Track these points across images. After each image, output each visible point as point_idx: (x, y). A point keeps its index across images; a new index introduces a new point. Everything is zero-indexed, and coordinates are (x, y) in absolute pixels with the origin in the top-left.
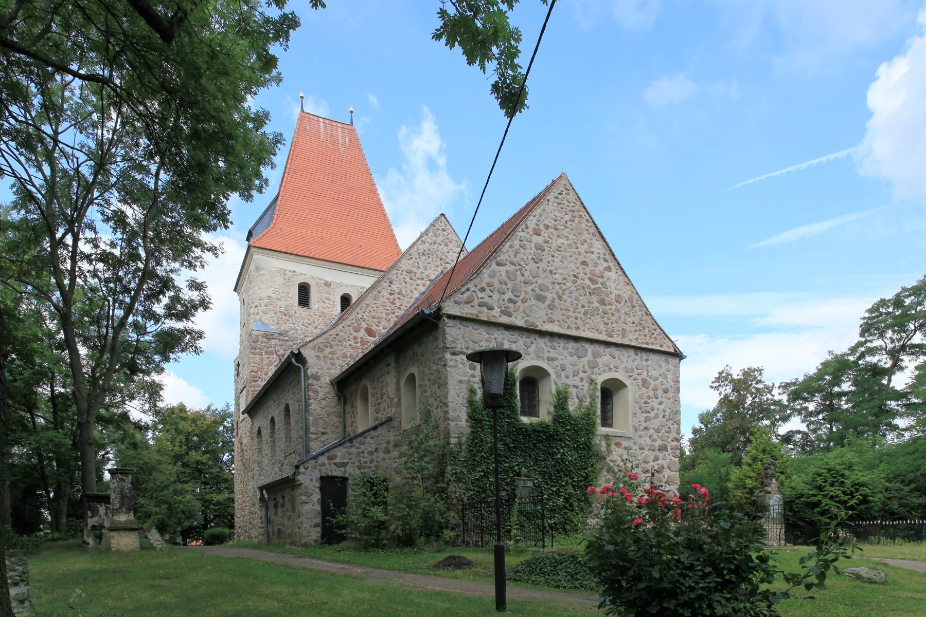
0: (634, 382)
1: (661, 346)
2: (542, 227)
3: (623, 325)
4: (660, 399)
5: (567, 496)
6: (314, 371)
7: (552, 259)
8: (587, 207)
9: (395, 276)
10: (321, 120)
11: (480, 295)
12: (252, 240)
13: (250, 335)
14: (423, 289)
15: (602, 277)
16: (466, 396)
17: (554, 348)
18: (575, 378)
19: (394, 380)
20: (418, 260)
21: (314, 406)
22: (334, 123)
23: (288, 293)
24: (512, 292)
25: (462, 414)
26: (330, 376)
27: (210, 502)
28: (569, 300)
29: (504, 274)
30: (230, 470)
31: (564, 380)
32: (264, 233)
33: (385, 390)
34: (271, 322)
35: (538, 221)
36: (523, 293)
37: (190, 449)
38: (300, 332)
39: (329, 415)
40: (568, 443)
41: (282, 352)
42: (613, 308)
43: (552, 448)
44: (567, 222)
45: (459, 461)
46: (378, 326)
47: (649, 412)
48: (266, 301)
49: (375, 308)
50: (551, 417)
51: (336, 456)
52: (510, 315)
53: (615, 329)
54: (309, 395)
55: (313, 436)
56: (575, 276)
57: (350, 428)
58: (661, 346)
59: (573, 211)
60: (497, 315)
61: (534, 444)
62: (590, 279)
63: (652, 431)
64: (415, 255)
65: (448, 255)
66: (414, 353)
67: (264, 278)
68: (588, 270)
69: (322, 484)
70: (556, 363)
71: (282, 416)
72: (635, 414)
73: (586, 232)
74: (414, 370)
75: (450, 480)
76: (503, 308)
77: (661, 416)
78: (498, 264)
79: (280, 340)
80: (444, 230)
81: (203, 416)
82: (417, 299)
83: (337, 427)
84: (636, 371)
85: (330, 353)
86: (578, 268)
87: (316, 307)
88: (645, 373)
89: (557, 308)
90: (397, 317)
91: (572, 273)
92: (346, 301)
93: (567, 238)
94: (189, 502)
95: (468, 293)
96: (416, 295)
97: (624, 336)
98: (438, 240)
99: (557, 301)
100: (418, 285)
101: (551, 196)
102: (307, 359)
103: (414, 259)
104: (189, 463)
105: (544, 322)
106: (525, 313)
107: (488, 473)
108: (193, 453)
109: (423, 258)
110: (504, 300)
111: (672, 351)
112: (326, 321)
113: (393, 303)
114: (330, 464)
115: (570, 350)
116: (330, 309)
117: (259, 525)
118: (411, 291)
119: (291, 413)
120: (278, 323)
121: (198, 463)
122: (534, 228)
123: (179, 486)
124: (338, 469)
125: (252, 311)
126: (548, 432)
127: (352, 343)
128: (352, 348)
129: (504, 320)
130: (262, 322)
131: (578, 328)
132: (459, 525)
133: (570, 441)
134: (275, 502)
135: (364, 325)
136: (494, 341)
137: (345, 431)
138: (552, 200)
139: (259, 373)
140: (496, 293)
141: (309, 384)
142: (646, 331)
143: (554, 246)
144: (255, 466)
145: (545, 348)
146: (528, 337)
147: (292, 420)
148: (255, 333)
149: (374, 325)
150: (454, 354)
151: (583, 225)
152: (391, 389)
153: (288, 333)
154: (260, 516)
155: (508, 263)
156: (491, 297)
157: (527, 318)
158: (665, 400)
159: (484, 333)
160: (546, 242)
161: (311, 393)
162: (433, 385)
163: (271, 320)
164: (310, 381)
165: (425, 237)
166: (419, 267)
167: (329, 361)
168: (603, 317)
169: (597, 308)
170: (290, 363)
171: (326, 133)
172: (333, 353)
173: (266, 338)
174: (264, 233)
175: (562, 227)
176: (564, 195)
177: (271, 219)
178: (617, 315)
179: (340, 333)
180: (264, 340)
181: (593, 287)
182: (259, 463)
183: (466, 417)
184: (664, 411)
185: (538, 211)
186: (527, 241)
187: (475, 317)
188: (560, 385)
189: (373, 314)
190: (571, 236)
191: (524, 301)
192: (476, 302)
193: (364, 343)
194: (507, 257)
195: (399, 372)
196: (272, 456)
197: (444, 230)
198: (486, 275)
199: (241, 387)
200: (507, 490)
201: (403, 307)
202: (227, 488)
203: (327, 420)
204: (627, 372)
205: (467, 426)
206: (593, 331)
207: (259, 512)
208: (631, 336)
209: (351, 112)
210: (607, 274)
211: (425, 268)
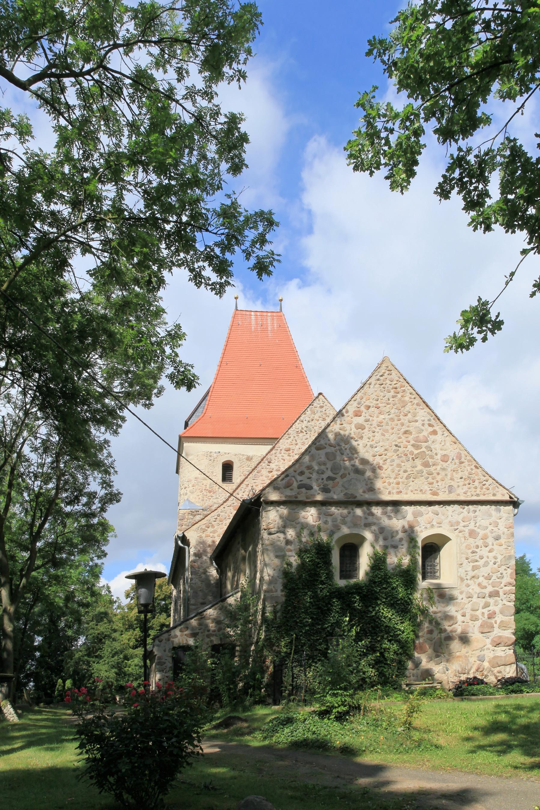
0: (460, 534)
1: (494, 495)
2: (362, 408)
3: (450, 481)
4: (490, 547)
8: (409, 382)
9: (273, 456)
11: (299, 478)
15: (426, 441)
23: (212, 472)
24: (331, 470)
28: (391, 468)
36: (343, 470)
42: (439, 467)
47: (477, 561)
48: (193, 482)
55: (193, 607)
56: (396, 446)
58: (494, 495)
63: (481, 579)
72: (461, 564)
77: (491, 563)
80: (322, 407)
84: (462, 524)
86: (400, 438)
88: (473, 523)
91: (394, 443)
93: (389, 413)
97: (450, 492)
98: (316, 417)
103: (292, 438)
106: (344, 487)
109: (301, 435)
110: (323, 479)
111: (507, 498)
120: (203, 500)
122: (355, 412)
130: (189, 501)
131: (401, 492)
142: (476, 483)
158: (496, 547)
160: (367, 421)
166: (297, 444)
168: (427, 478)
169: (421, 470)
171: (257, 324)
178: (443, 473)
179: (221, 514)
181: (416, 452)
183: (282, 588)
184: (495, 558)
187: (294, 499)
191: (343, 476)
197: (322, 407)
204: (452, 526)
205: (282, 595)
206: (416, 492)
210: (432, 437)
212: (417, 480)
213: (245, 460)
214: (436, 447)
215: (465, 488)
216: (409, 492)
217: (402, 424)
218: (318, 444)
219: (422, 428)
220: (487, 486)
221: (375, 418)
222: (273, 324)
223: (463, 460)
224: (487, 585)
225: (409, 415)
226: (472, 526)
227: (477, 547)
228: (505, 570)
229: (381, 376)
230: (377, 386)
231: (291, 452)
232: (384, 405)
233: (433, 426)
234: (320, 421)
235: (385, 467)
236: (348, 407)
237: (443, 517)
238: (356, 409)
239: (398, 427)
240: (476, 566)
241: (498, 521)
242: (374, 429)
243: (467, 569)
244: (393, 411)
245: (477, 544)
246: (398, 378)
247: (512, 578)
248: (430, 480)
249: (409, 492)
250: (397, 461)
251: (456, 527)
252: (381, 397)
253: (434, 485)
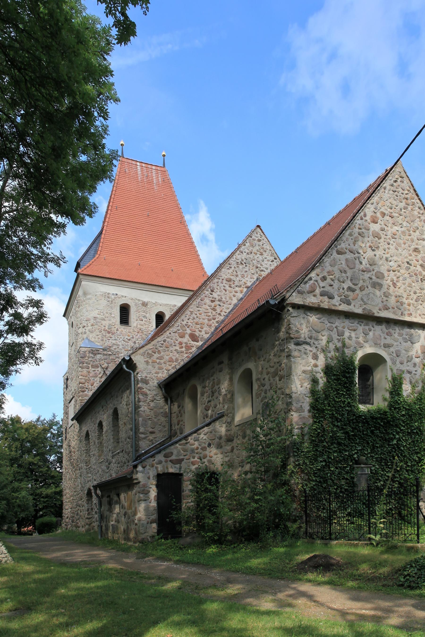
2: (378, 215)
5: (402, 481)
6: (144, 376)
7: (388, 246)
8: (419, 194)
9: (216, 284)
10: (138, 164)
11: (322, 284)
12: (79, 271)
13: (79, 352)
14: (241, 296)
16: (309, 386)
18: (409, 363)
19: (228, 377)
20: (237, 269)
21: (144, 408)
22: (149, 166)
23: (111, 314)
24: (351, 280)
25: (304, 404)
26: (158, 380)
27: (40, 495)
28: (403, 287)
29: (344, 262)
30: (56, 468)
31: (399, 366)
32: (91, 262)
33: (216, 387)
34: (97, 340)
35: (376, 209)
37: (23, 453)
38: (121, 347)
39: (156, 416)
40: (402, 428)
41: (105, 365)
43: (388, 434)
44: (401, 209)
45: (302, 452)
46: (200, 331)
49: (198, 315)
50: (386, 403)
51: (172, 453)
52: (349, 304)
54: (139, 398)
55: (142, 436)
56: (408, 263)
57: (177, 427)
59: (407, 199)
60: (337, 304)
61: (372, 432)
62: (421, 265)
64: (234, 264)
65: (262, 263)
66: (250, 349)
67: (91, 302)
68: (419, 256)
69: (158, 481)
70: (392, 349)
71: (111, 419)
73: (418, 219)
74: (251, 365)
75: (293, 472)
76: (343, 297)
78: (339, 253)
79: (104, 355)
80: (259, 241)
81: (34, 425)
82: (236, 305)
83: (164, 426)
85: (157, 359)
86: (410, 255)
87: (135, 325)
89: (391, 296)
90: (217, 322)
91: (406, 260)
92: (160, 317)
94: (23, 497)
95: (312, 282)
96: (235, 301)
98: (254, 250)
99: (392, 287)
100: (236, 292)
101: (387, 184)
102: (138, 365)
103: (233, 268)
104: (23, 464)
105: (380, 310)
106: (363, 301)
107: (329, 462)
108: (26, 456)
109: (241, 267)
112: (143, 336)
113: (214, 310)
114: (166, 462)
115: (404, 336)
116: (147, 326)
117: (86, 516)
118: (230, 298)
119: (120, 416)
120: (102, 340)
121: (31, 463)
123: (16, 484)
124: (173, 466)
125: (80, 331)
126: (385, 419)
127: (177, 348)
128: (178, 352)
129: (343, 307)
130: (89, 340)
131: (411, 314)
132: (301, 517)
133: (404, 427)
134: (108, 499)
135: (188, 331)
136: (335, 329)
137: (171, 430)
138: (388, 187)
139: (86, 384)
140: (336, 281)
141: (140, 388)
143: (389, 233)
144: (83, 465)
145: (382, 334)
146: (367, 325)
147: (121, 423)
148: (83, 349)
149: (197, 330)
150: (298, 344)
151: (416, 213)
152: (224, 387)
153: (111, 348)
154: (86, 508)
155: (347, 251)
156: (331, 285)
157: (364, 306)
159: (326, 322)
160: (383, 230)
161: (141, 397)
162: (274, 377)
163: (97, 337)
164: (140, 385)
165: (243, 247)
167: (157, 366)
170: (122, 368)
171: (143, 175)
172: (161, 358)
173: (92, 353)
174: (91, 262)
175: (397, 215)
176: (399, 183)
177: (96, 251)
179: (167, 340)
180: (91, 355)
182: (87, 463)
183: (309, 408)
185: (375, 199)
186: (365, 228)
188: (395, 371)
189: (197, 320)
190: (405, 224)
191: (362, 289)
192: (318, 291)
193: (188, 347)
194: (347, 246)
195: (232, 370)
196: (99, 456)
197: (259, 241)
198: (327, 264)
199: (69, 397)
200: (347, 479)
201: (223, 314)
202: (53, 483)
203: (155, 420)
205: (309, 416)
207: (86, 505)
209: (164, 156)
211: (243, 276)
213: (140, 305)
217: (412, 241)
221: (389, 228)
230: (391, 192)
231: (231, 283)
234: (258, 255)
242: (388, 240)
246: (408, 188)
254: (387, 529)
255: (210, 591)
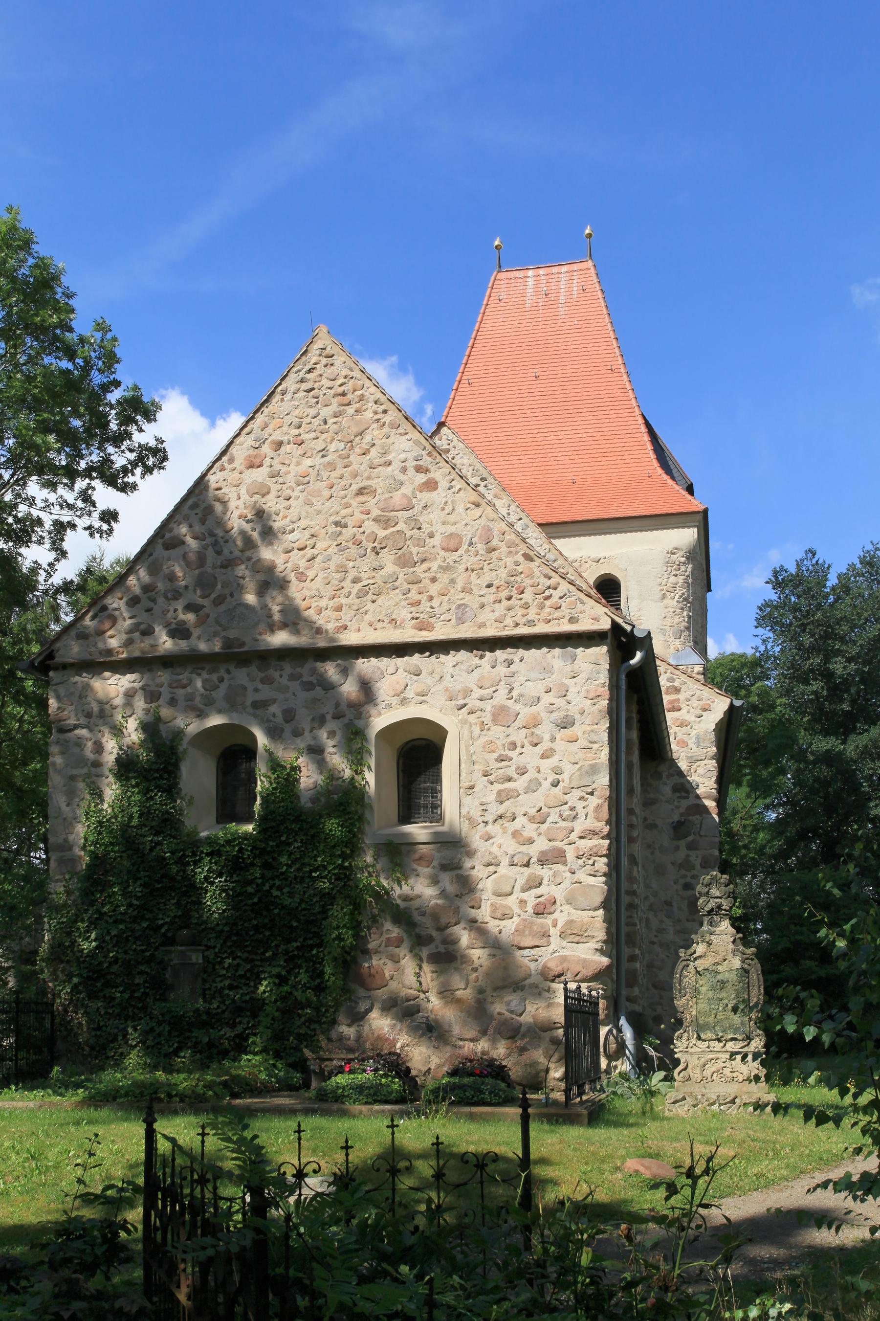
0: (472, 718)
2: (266, 449)
3: (462, 595)
4: (546, 745)
17: (268, 681)
28: (322, 575)
42: (434, 566)
47: (510, 779)
53: (437, 611)
56: (337, 524)
58: (572, 620)
63: (520, 821)
70: (274, 709)
72: (472, 787)
77: (546, 784)
86: (347, 506)
88: (503, 691)
93: (324, 453)
97: (461, 621)
106: (221, 626)
115: (305, 679)
142: (528, 596)
143: (290, 479)
146: (214, 670)
178: (444, 578)
181: (382, 533)
184: (558, 771)
206: (380, 625)
208: (486, 616)
210: (425, 497)
212: (382, 597)
214: (433, 519)
215: (500, 609)
216: (364, 626)
218: (168, 535)
219: (402, 477)
220: (555, 599)
222: (569, 290)
223: (495, 543)
224: (534, 835)
225: (374, 452)
226: (500, 698)
227: (513, 746)
228: (581, 798)
229: (310, 371)
230: (302, 394)
232: (313, 435)
233: (427, 471)
235: (311, 574)
236: (234, 450)
237: (430, 681)
238: (251, 452)
239: (343, 482)
240: (508, 790)
241: (567, 682)
243: (484, 800)
244: (332, 447)
245: (511, 739)
247: (597, 819)
248: (414, 596)
249: (364, 626)
250: (337, 560)
251: (461, 702)
252: (308, 420)
253: (421, 608)
254: (826, 1026)
255: (299, 1107)
